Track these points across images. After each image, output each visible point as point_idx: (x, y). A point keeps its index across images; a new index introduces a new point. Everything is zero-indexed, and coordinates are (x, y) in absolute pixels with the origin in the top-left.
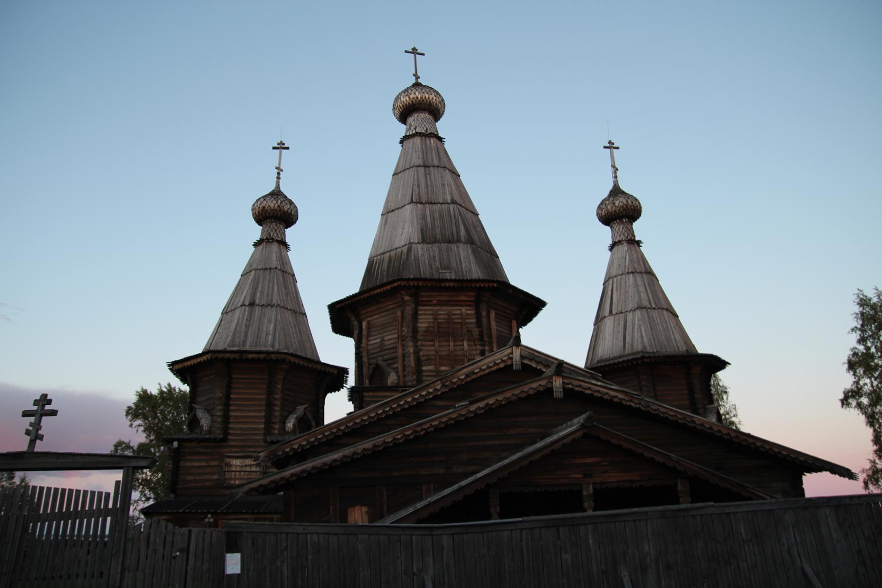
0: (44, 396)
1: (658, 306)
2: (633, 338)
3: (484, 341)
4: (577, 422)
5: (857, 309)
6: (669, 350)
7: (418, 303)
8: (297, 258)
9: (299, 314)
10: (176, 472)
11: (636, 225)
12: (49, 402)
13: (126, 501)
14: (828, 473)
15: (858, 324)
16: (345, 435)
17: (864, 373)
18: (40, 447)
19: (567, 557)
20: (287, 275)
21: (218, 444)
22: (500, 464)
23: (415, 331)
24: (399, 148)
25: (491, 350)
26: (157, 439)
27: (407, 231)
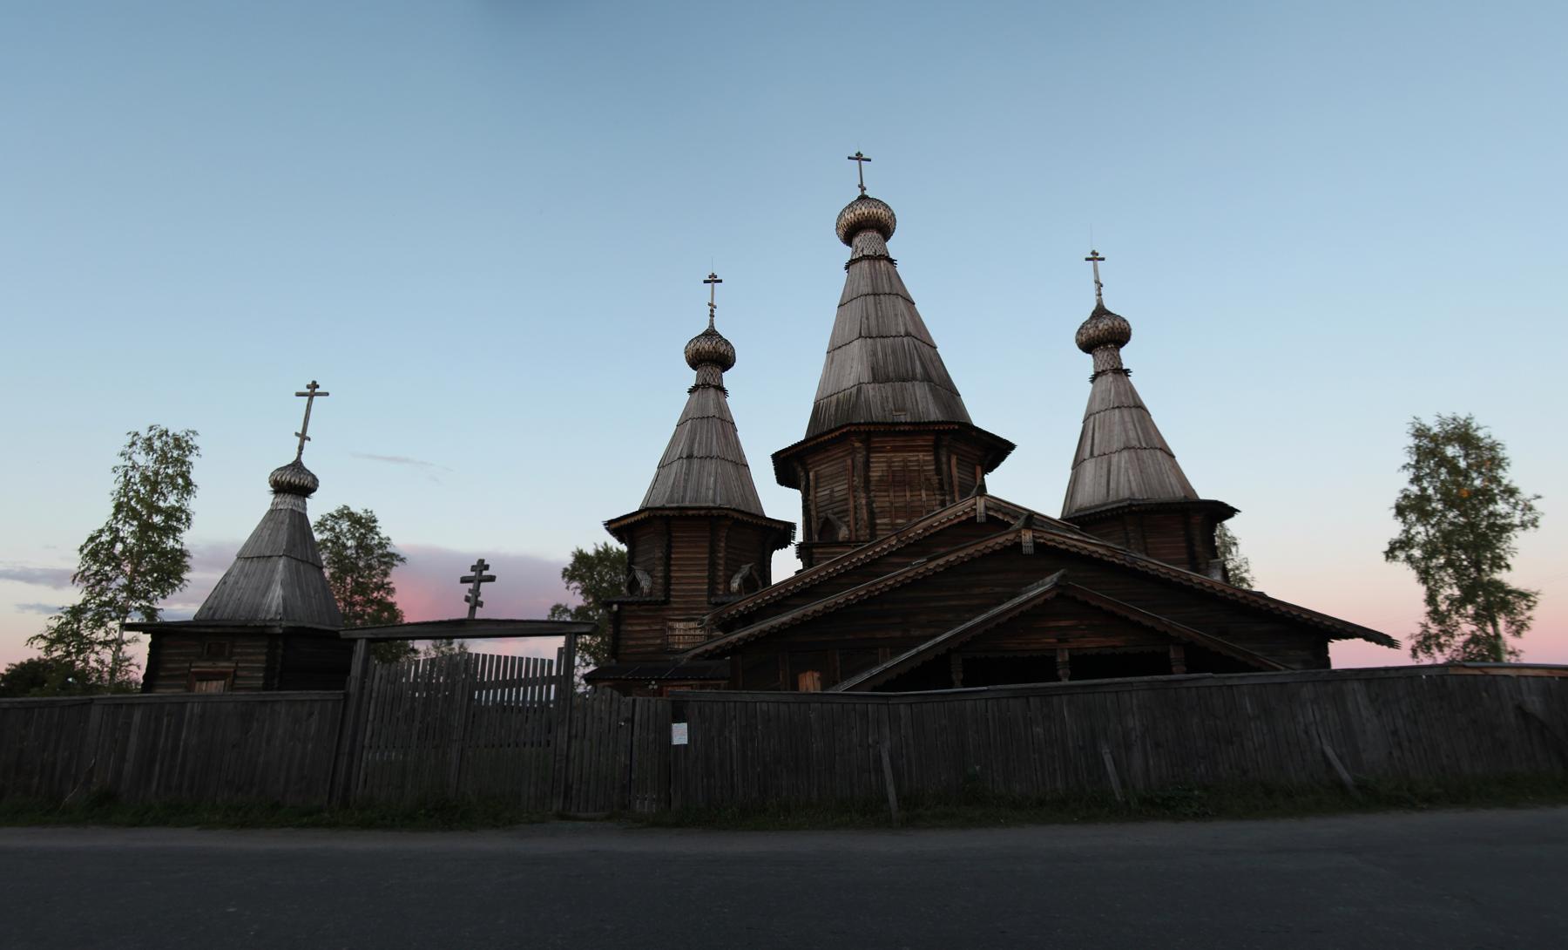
0: (481, 561)
1: (1150, 444)
2: (1118, 483)
3: (945, 490)
4: (1050, 581)
5: (1412, 442)
7: (869, 450)
8: (736, 404)
9: (741, 465)
10: (616, 637)
11: (1125, 352)
12: (487, 567)
13: (570, 666)
14: (1361, 640)
15: (1412, 460)
16: (794, 595)
17: (1418, 520)
18: (480, 614)
19: (1039, 730)
20: (725, 424)
21: (659, 606)
22: (962, 627)
23: (867, 480)
24: (845, 274)
25: (953, 501)
26: (595, 601)
27: (856, 370)
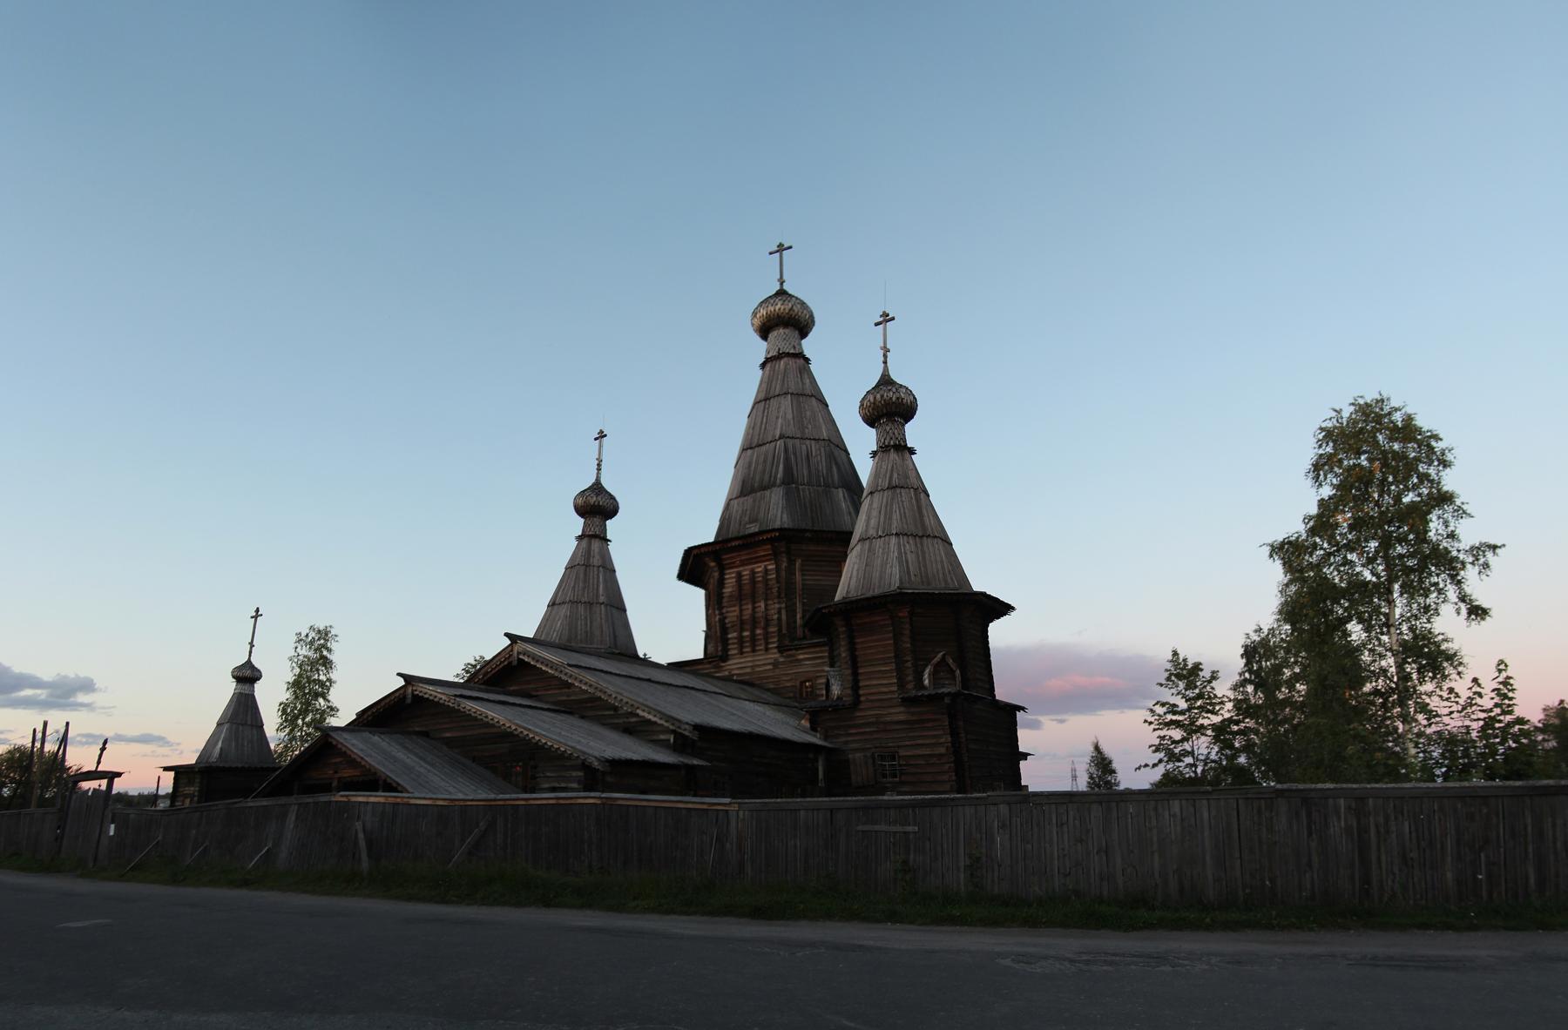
6: (937, 587)
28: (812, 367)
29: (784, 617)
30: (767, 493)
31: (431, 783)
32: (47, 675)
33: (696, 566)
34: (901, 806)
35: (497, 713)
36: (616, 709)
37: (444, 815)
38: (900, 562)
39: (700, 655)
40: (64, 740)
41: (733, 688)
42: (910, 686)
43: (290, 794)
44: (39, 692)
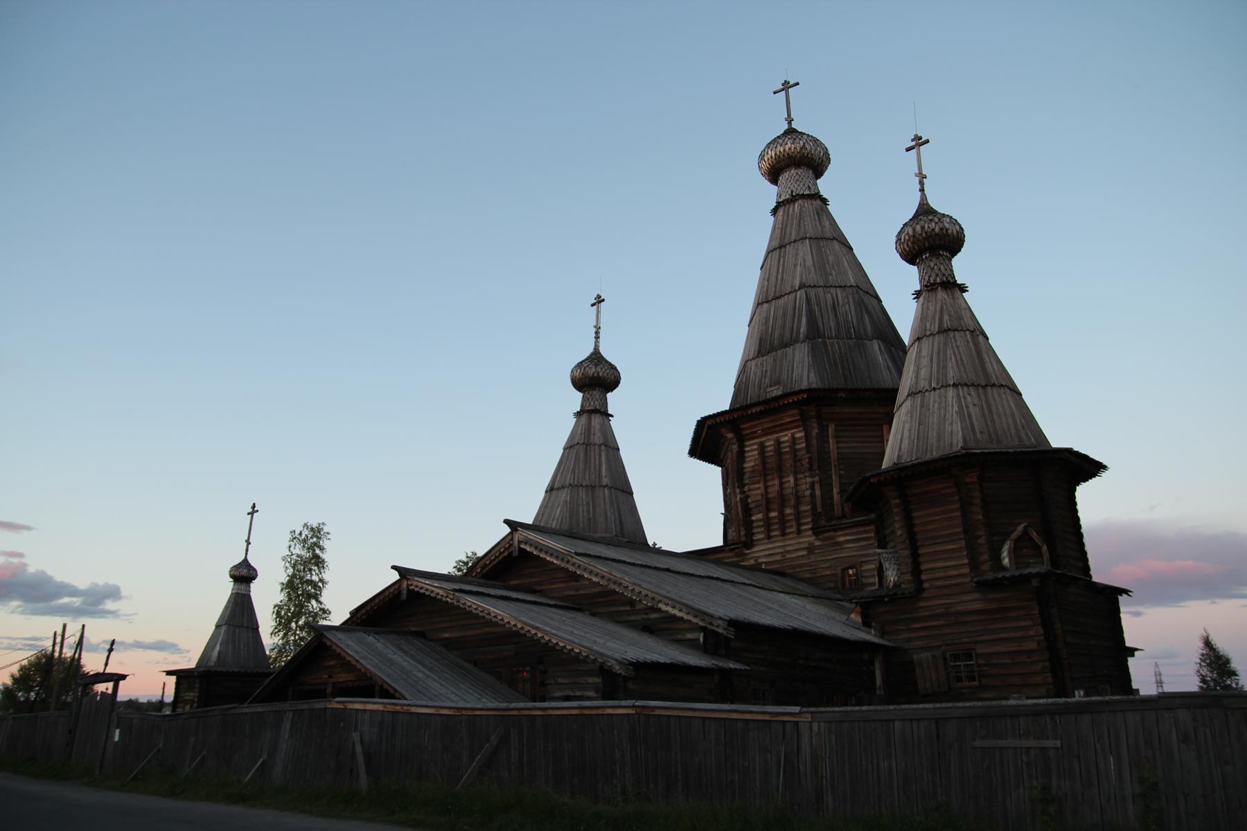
6: (1010, 444)
28: (831, 208)
29: (818, 492)
30: (789, 350)
31: (434, 690)
32: (82, 584)
33: (709, 441)
34: (1036, 713)
35: (500, 610)
36: (632, 603)
37: (450, 726)
38: (962, 420)
39: (719, 542)
40: (80, 644)
41: (763, 579)
42: (986, 567)
43: (285, 700)
44: (74, 599)
